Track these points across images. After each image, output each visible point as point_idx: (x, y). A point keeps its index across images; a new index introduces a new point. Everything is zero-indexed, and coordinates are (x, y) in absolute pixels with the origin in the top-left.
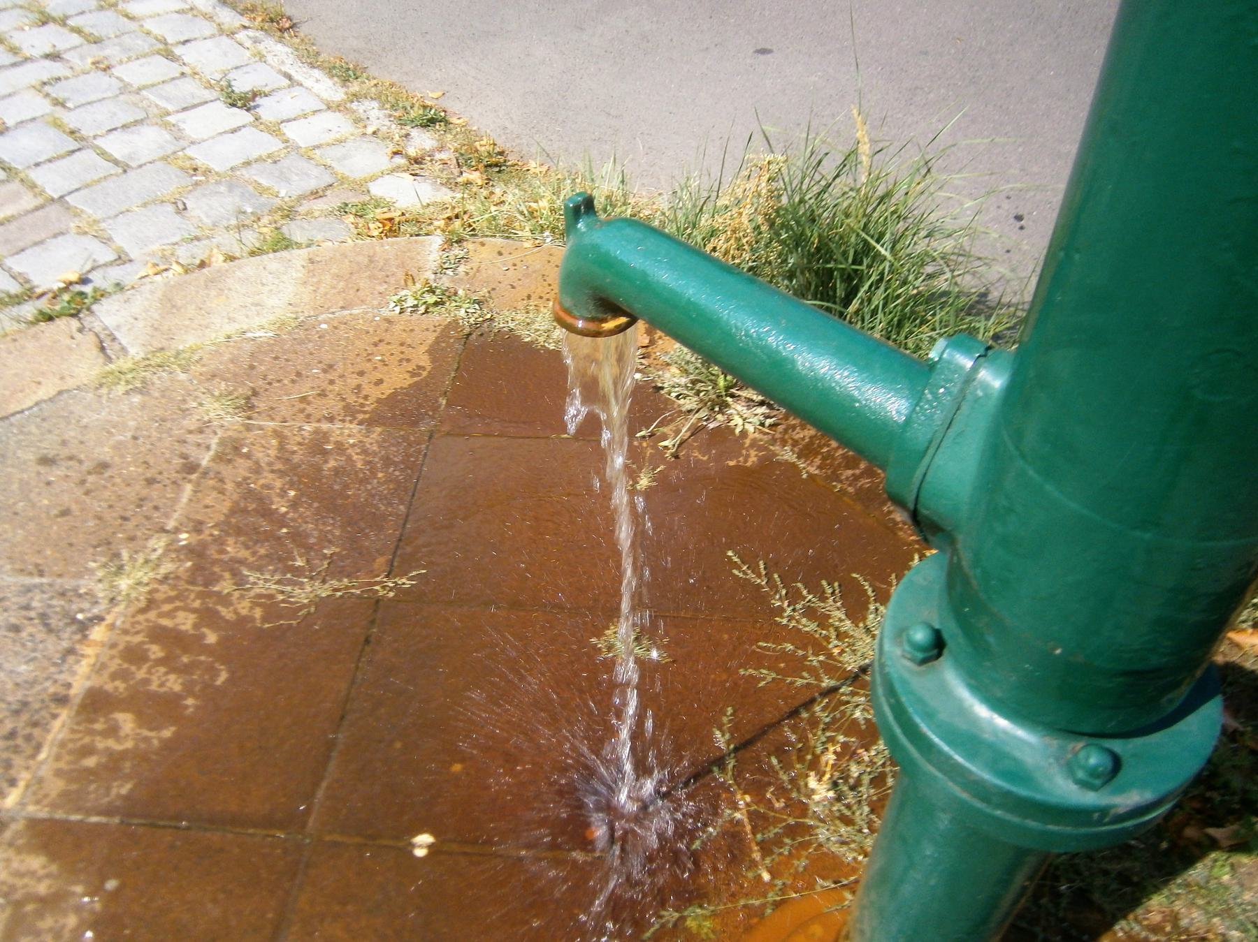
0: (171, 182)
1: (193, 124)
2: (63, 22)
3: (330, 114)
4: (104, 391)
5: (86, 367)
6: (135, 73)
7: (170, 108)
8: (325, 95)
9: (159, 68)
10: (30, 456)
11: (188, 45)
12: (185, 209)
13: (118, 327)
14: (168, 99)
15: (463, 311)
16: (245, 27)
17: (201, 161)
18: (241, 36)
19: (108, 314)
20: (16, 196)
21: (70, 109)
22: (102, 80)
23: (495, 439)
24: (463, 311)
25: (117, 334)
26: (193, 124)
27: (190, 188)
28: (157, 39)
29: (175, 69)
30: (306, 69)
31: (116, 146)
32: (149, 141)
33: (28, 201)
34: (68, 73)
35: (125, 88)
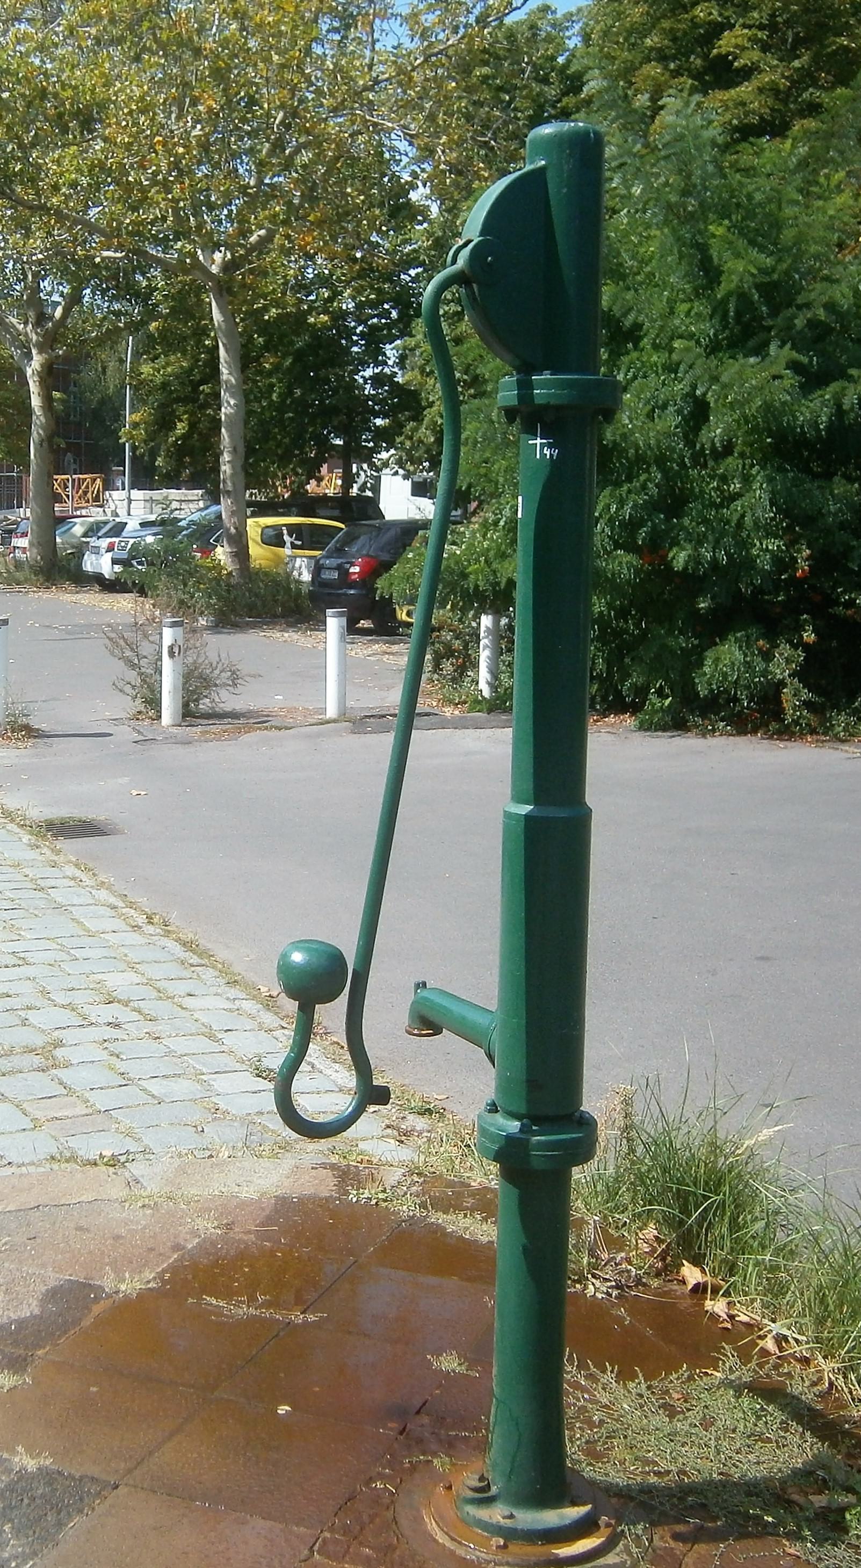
0: (196, 1116)
1: (221, 1083)
2: (126, 1004)
3: (340, 1094)
4: (127, 1205)
5: (116, 1191)
6: (180, 1045)
7: (204, 1071)
8: (340, 1082)
9: (202, 1044)
10: (72, 1225)
11: (229, 1033)
12: (203, 1131)
13: (143, 1176)
14: (204, 1064)
15: (405, 1207)
16: (283, 1028)
17: (222, 1106)
18: (278, 1033)
19: (137, 1169)
20: (74, 1105)
21: (122, 1060)
22: (155, 1044)
23: (91, 599)
24: (405, 1207)
25: (141, 1180)
26: (221, 1083)
27: (123, 1159)
28: (203, 1024)
29: (216, 1047)
30: (329, 1062)
31: (155, 1087)
32: (183, 1088)
33: (81, 1109)
34: (126, 1037)
35: (170, 1053)
